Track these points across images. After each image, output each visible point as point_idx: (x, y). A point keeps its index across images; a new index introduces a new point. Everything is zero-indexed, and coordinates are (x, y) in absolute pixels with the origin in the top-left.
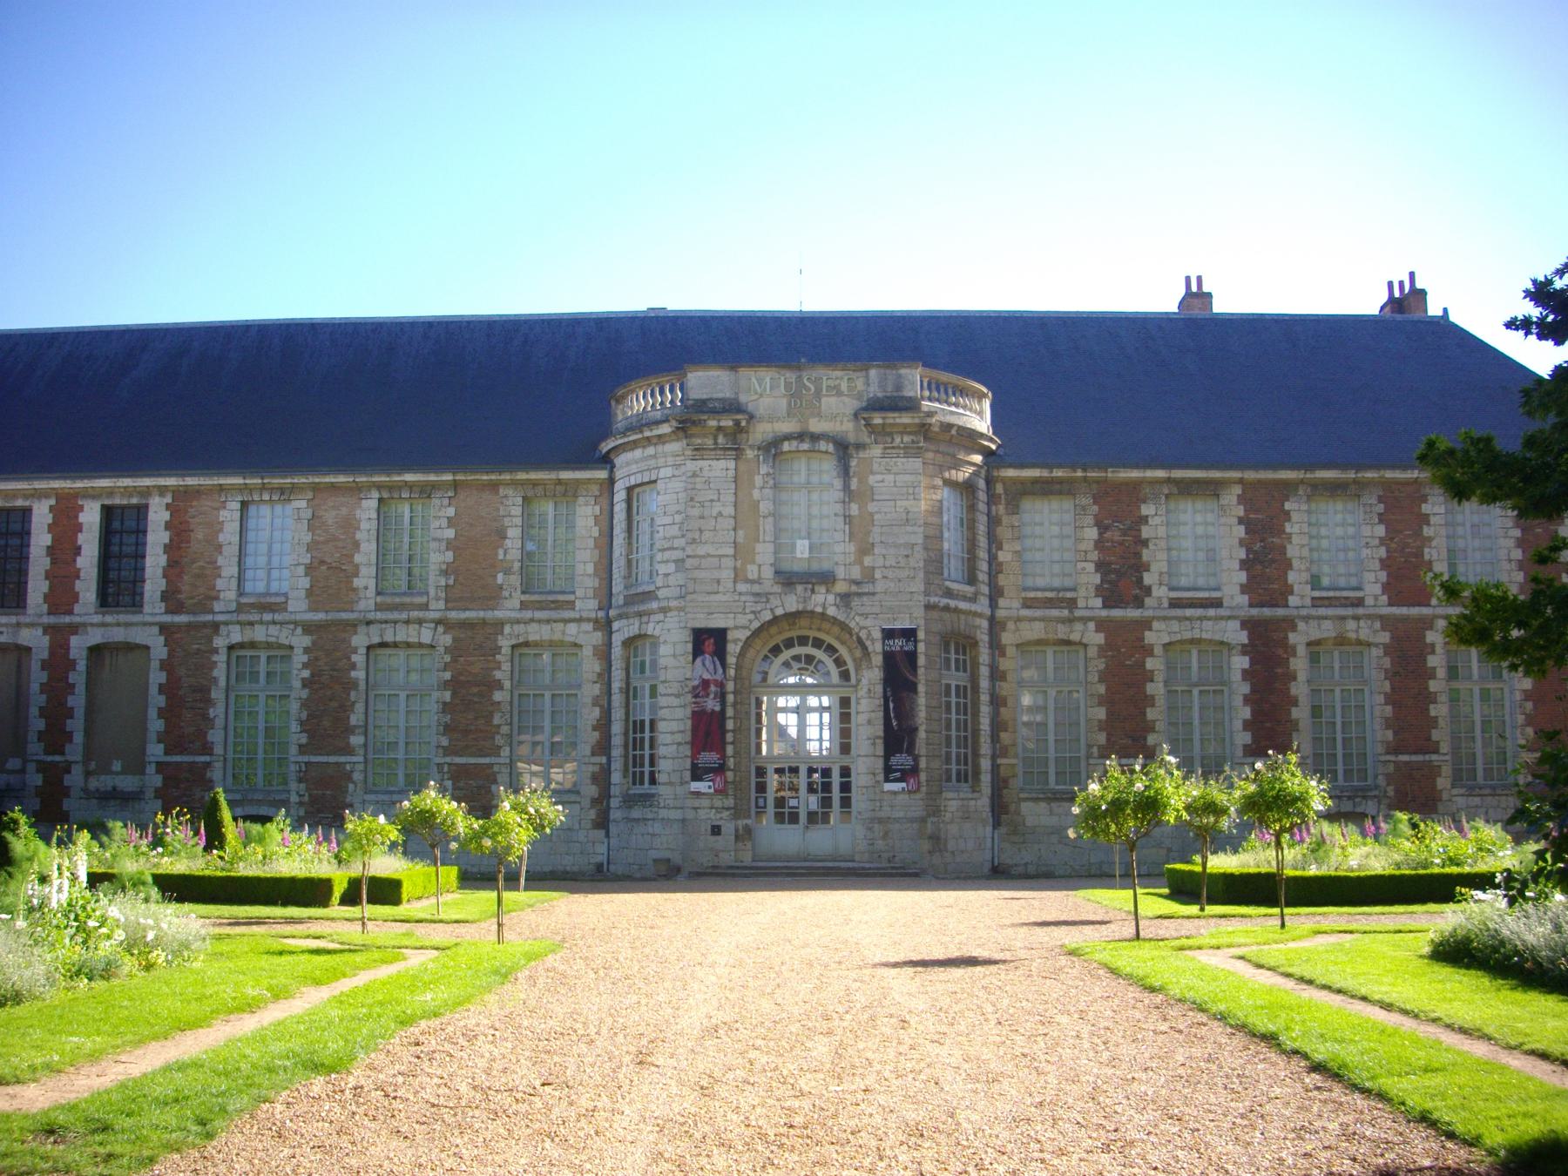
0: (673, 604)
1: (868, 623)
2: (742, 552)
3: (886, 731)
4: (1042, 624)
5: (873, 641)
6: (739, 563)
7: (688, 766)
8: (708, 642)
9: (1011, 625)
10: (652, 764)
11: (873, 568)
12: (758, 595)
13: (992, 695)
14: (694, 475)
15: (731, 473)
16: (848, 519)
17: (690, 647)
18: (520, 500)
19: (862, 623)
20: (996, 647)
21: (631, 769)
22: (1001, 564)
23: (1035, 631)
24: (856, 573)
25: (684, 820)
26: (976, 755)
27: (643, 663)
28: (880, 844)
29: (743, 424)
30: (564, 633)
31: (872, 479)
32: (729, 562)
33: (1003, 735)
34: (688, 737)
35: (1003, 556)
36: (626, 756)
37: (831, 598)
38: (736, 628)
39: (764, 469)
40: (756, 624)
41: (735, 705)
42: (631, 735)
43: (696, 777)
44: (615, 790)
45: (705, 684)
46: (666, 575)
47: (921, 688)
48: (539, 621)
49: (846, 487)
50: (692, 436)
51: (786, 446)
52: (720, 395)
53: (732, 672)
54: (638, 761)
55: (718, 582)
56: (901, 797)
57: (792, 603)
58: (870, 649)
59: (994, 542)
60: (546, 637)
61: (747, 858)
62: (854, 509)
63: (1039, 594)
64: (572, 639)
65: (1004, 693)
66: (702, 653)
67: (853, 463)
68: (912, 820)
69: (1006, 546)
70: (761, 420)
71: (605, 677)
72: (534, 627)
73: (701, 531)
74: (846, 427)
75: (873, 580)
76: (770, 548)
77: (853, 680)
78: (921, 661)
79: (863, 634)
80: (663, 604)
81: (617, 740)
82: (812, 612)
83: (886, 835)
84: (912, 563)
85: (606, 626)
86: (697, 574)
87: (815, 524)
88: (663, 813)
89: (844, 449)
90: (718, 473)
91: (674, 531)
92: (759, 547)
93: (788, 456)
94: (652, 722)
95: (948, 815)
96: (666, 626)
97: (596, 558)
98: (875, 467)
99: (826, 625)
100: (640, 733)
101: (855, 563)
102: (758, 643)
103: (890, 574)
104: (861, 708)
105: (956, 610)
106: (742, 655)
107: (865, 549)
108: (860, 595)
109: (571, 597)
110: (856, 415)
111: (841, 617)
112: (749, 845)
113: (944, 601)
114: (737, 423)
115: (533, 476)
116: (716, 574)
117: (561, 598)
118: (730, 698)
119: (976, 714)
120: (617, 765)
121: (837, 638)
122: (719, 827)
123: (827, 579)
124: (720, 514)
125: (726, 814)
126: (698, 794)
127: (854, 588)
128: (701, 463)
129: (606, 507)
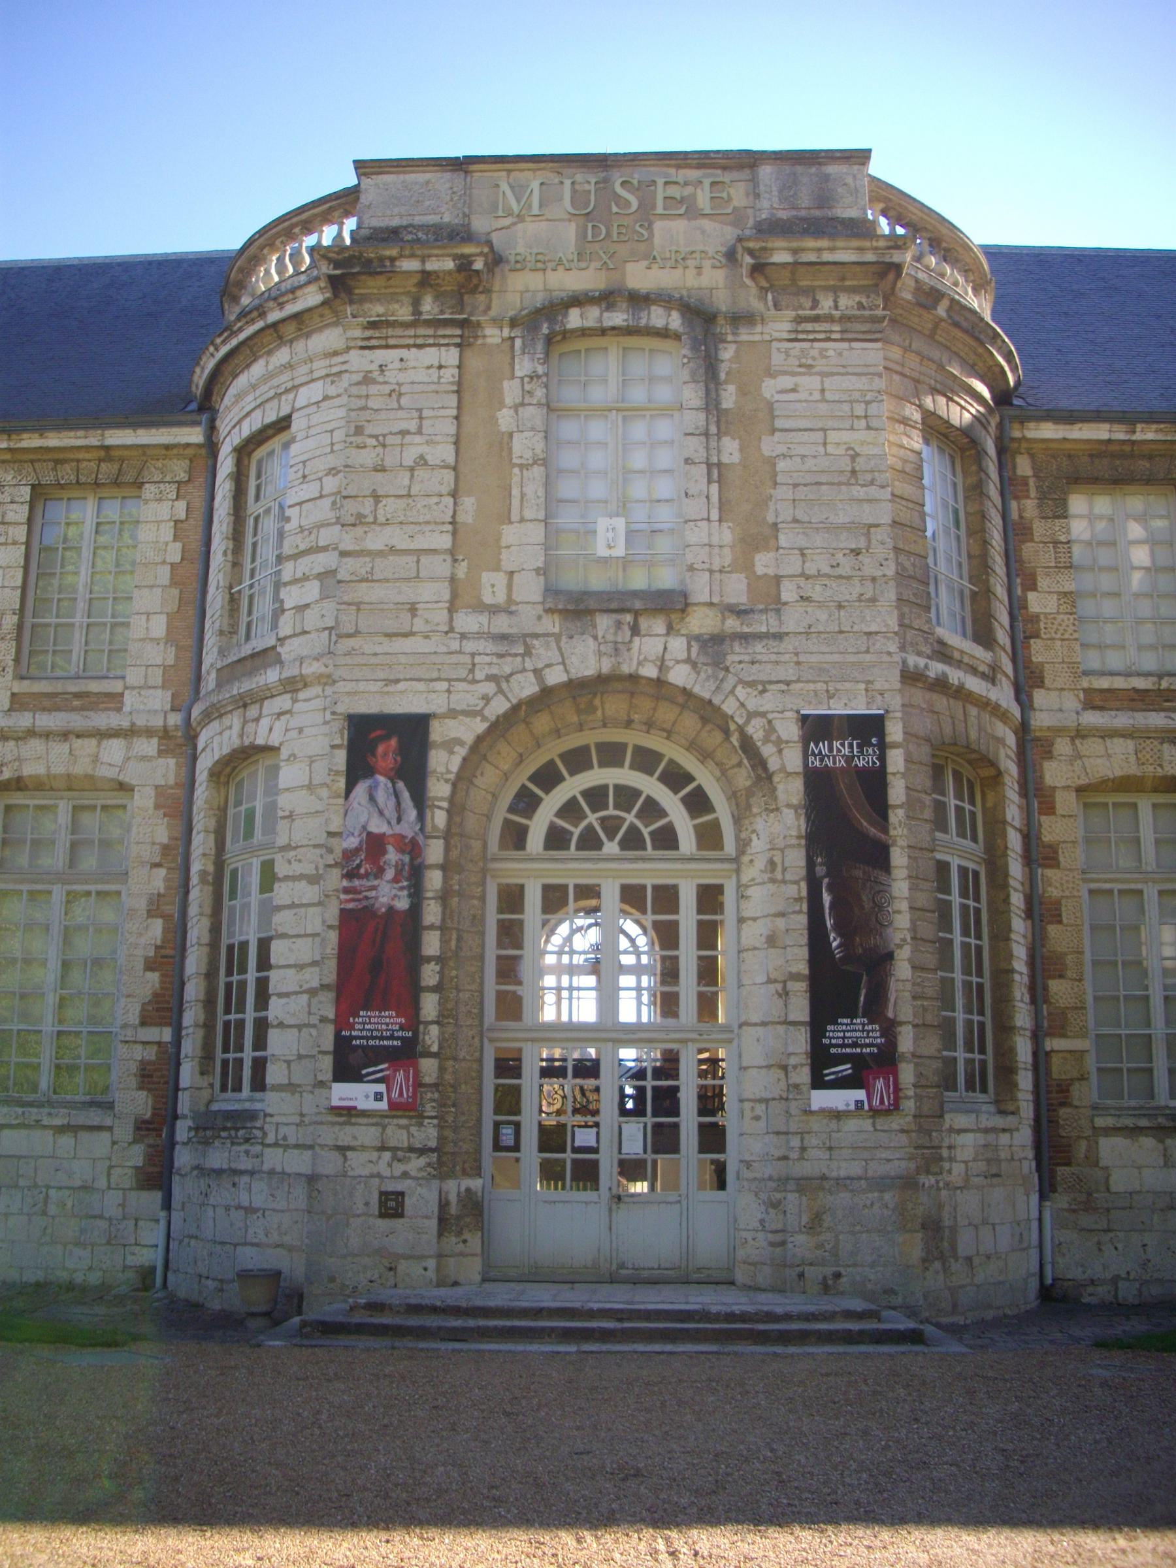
0: (311, 669)
1: (767, 703)
2: (468, 545)
3: (813, 961)
4: (1130, 744)
5: (780, 744)
6: (462, 570)
7: (328, 1043)
8: (384, 746)
9: (1062, 747)
10: (260, 1042)
11: (778, 579)
12: (504, 637)
13: (1029, 899)
14: (367, 380)
15: (450, 374)
16: (716, 471)
17: (341, 758)
18: (26, 492)
19: (751, 705)
20: (1037, 796)
21: (219, 1055)
22: (1035, 619)
23: (1115, 759)
24: (736, 590)
25: (312, 1179)
26: (1004, 1028)
27: (250, 816)
28: (801, 1244)
29: (478, 265)
30: (96, 759)
31: (769, 388)
32: (440, 566)
33: (1055, 986)
34: (330, 973)
35: (1036, 602)
36: (208, 1027)
37: (678, 646)
38: (453, 714)
39: (524, 366)
40: (500, 706)
41: (444, 897)
42: (222, 979)
43: (346, 1071)
44: (184, 1104)
45: (375, 845)
46: (302, 608)
47: (899, 858)
48: (47, 735)
49: (712, 404)
50: (364, 299)
51: (574, 319)
52: (432, 219)
53: (439, 818)
54: (233, 1035)
55: (413, 610)
56: (851, 1125)
57: (585, 658)
58: (773, 764)
59: (1022, 577)
60: (59, 769)
61: (470, 1289)
62: (730, 451)
63: (1119, 683)
64: (111, 773)
65: (1054, 892)
67: (727, 353)
68: (881, 1184)
69: (1043, 583)
70: (520, 266)
71: (177, 854)
72: (36, 746)
73: (377, 498)
74: (710, 281)
75: (777, 606)
76: (536, 533)
77: (730, 847)
78: (897, 792)
79: (755, 730)
80: (291, 671)
81: (194, 990)
82: (633, 678)
83: (815, 1224)
84: (870, 569)
85: (183, 743)
86: (364, 592)
87: (638, 490)
88: (273, 1159)
89: (704, 324)
90: (421, 376)
91: (323, 511)
92: (510, 534)
93: (582, 344)
94: (264, 945)
95: (958, 1169)
96: (295, 722)
97: (173, 606)
98: (777, 359)
99: (666, 714)
100: (239, 974)
101: (735, 567)
102: (505, 754)
103: (816, 591)
104: (749, 909)
105: (960, 693)
106: (463, 779)
107: (760, 536)
108: (745, 638)
109: (117, 687)
110: (731, 256)
111: (703, 690)
112: (475, 1242)
113: (937, 668)
114: (464, 265)
115: (53, 440)
116: (408, 593)
117: (94, 687)
118: (434, 880)
119: (1001, 935)
120: (190, 1046)
121: (693, 746)
123: (670, 605)
124: (422, 461)
125: (416, 1164)
126: (349, 1113)
127: (732, 624)
128: (381, 355)
129: (199, 504)
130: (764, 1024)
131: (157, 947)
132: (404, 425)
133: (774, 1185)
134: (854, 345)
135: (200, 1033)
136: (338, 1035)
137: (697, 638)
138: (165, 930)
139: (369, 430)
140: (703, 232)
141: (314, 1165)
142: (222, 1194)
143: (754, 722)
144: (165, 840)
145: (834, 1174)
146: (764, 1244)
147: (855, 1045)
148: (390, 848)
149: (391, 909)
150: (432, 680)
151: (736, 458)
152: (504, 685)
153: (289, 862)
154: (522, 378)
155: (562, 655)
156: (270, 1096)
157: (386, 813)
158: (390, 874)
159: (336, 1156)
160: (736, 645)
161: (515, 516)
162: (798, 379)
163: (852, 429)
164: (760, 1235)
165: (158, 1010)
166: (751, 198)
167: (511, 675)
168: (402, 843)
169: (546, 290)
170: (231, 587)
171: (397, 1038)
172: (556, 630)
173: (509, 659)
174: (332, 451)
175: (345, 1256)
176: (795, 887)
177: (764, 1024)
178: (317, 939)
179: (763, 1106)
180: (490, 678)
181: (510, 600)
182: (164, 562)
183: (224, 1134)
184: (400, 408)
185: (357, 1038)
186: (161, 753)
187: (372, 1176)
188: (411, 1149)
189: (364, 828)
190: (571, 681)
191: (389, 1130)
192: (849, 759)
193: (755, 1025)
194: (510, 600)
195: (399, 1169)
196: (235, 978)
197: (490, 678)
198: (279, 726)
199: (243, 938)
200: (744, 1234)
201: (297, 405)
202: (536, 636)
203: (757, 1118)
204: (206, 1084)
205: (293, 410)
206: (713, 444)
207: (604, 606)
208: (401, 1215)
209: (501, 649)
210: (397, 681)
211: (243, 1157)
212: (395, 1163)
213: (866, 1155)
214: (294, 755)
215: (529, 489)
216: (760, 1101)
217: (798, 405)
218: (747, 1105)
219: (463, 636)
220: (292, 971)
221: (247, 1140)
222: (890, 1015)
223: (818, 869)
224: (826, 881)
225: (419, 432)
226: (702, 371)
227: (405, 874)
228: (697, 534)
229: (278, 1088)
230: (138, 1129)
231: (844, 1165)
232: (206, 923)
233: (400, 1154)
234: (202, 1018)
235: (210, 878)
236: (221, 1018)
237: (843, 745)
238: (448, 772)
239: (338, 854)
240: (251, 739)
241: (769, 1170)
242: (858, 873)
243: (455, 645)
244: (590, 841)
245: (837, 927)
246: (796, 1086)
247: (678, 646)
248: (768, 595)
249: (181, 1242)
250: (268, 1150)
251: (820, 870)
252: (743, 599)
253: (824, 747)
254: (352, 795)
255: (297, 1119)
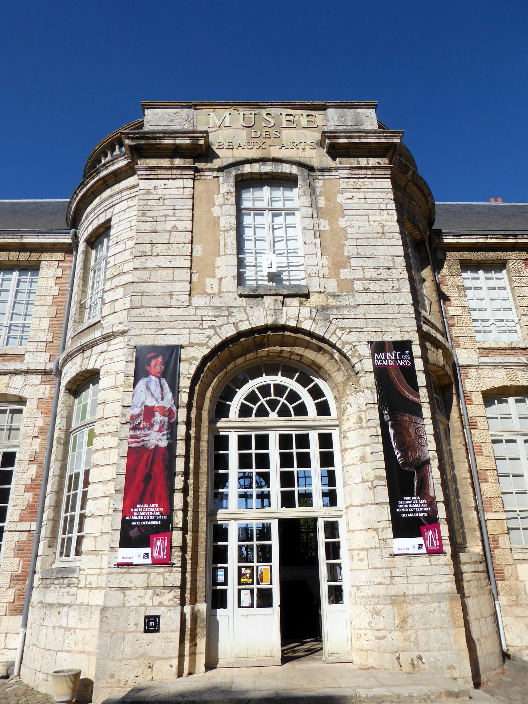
1: (353, 337)
16: (318, 233)
17: (132, 367)
19: (345, 338)
23: (497, 379)
24: (332, 286)
31: (340, 198)
36: (55, 521)
38: (191, 345)
40: (216, 341)
45: (149, 412)
49: (314, 204)
53: (184, 398)
57: (259, 316)
62: (324, 225)
66: (147, 374)
69: (454, 302)
84: (396, 276)
94: (87, 472)
96: (108, 355)
103: (372, 286)
104: (348, 444)
107: (340, 263)
108: (338, 307)
111: (319, 331)
116: (168, 287)
118: (181, 430)
122: (156, 619)
124: (175, 229)
127: (331, 301)
130: (362, 505)
131: (32, 480)
132: (166, 212)
133: (376, 600)
134: (377, 180)
135: (50, 523)
136: (124, 520)
137: (315, 307)
138: (38, 471)
139: (149, 214)
140: (305, 135)
141: (105, 600)
142: (52, 619)
143: (346, 347)
144: (41, 425)
145: (411, 593)
146: (373, 638)
147: (414, 512)
148: (157, 414)
149: (157, 446)
150: (180, 329)
151: (327, 228)
152: (218, 331)
153: (102, 426)
154: (223, 194)
155: (248, 316)
156: (82, 558)
157: (155, 395)
158: (157, 427)
159: (119, 594)
160: (334, 310)
161: (222, 252)
162: (353, 194)
163: (381, 214)
164: (369, 632)
165: (30, 513)
166: (325, 121)
167: (222, 325)
168: (164, 411)
169: (233, 157)
170: (81, 301)
171: (158, 520)
172: (244, 304)
173: (220, 318)
174: (131, 230)
175: (121, 661)
176: (375, 429)
177: (362, 505)
178: (115, 466)
179: (365, 552)
180: (210, 327)
181: (220, 291)
182: (50, 295)
183: (56, 582)
184: (164, 205)
185: (134, 521)
186: (42, 383)
187: (140, 606)
188: (165, 587)
189: (143, 403)
190: (252, 328)
191: (152, 576)
192: (396, 361)
193: (357, 506)
194: (220, 291)
195: (157, 600)
196: (72, 492)
197: (210, 327)
198: (101, 358)
199: (77, 471)
200: (360, 632)
201: (114, 213)
202: (234, 307)
203: (362, 560)
204: (51, 553)
205: (113, 215)
206: (316, 221)
207: (268, 292)
208: (158, 631)
209: (216, 314)
210: (163, 329)
211: (66, 596)
212: (155, 596)
213: (427, 579)
214: (107, 372)
215: (229, 241)
216: (363, 550)
217: (354, 205)
218: (355, 553)
219: (197, 307)
220: (101, 485)
221: (69, 585)
222: (432, 494)
223: (385, 416)
224: (390, 423)
225: (174, 215)
226: (308, 191)
227: (165, 427)
228: (312, 261)
229: (90, 553)
230: (12, 580)
231: (415, 586)
232: (59, 464)
233: (158, 590)
234: (52, 516)
235: (62, 441)
236: (63, 515)
237: (391, 355)
238: (189, 374)
239: (128, 418)
240: (86, 367)
241: (371, 591)
242: (406, 418)
243: (193, 312)
244: (262, 413)
245: (398, 447)
246: (385, 540)
247: (305, 311)
248: (347, 287)
249: (29, 647)
250: (80, 591)
251: (387, 418)
252: (336, 290)
253: (382, 356)
254: (137, 386)
255: (98, 571)
